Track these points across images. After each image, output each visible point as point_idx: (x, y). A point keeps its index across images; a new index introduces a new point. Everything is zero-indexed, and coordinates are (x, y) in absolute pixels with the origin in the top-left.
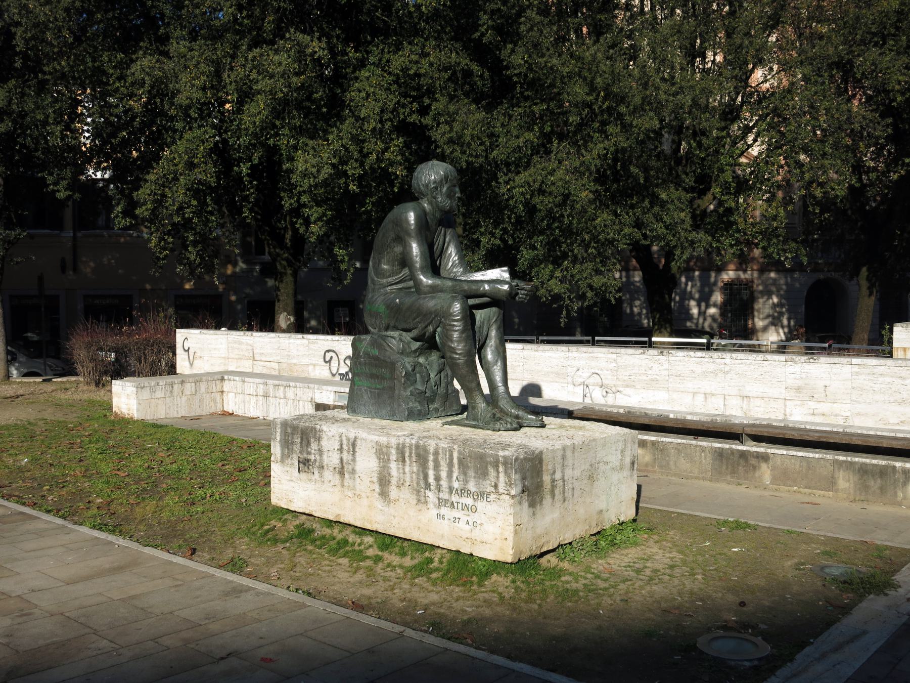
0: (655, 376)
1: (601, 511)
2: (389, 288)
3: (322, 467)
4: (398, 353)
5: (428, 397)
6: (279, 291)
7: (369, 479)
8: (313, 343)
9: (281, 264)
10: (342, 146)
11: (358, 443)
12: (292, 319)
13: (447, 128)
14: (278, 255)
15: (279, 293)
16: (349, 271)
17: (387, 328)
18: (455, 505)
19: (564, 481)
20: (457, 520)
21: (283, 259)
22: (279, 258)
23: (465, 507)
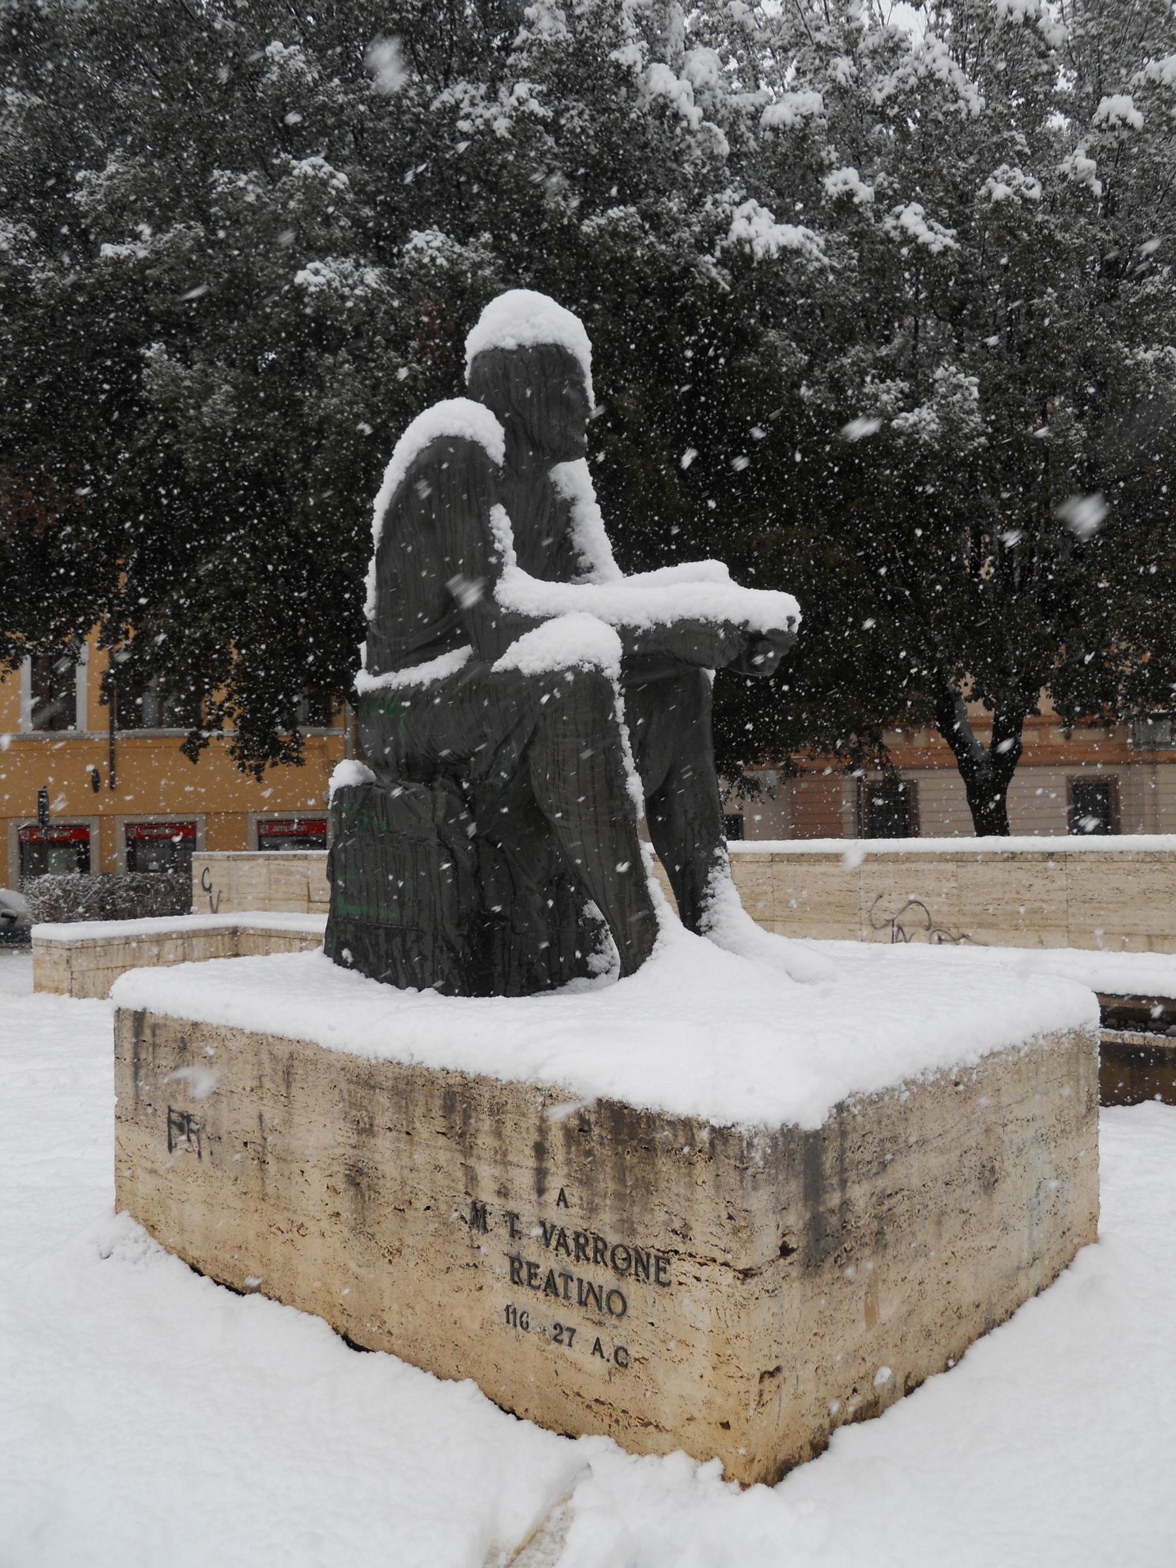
0: (1039, 904)
7: (327, 1181)
18: (559, 1282)
20: (565, 1336)
23: (590, 1295)
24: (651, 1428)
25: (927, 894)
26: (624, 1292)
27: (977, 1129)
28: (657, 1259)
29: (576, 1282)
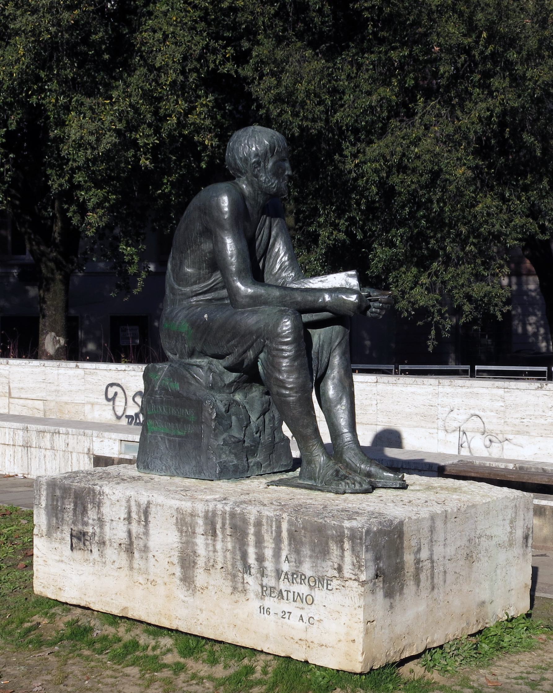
1: (484, 603)
2: (195, 299)
3: (102, 543)
4: (207, 387)
5: (247, 447)
6: (45, 302)
8: (91, 374)
9: (47, 266)
10: (131, 105)
11: (153, 509)
12: (62, 341)
13: (274, 81)
14: (43, 254)
15: (44, 306)
16: (140, 276)
17: (192, 354)
18: (285, 594)
19: (432, 562)
20: (287, 615)
21: (50, 260)
22: (44, 259)
24: (323, 647)
25: (484, 410)
26: (313, 595)
27: (465, 539)
28: (327, 580)
29: (292, 593)
